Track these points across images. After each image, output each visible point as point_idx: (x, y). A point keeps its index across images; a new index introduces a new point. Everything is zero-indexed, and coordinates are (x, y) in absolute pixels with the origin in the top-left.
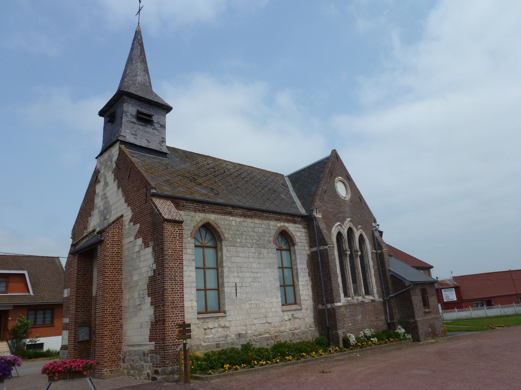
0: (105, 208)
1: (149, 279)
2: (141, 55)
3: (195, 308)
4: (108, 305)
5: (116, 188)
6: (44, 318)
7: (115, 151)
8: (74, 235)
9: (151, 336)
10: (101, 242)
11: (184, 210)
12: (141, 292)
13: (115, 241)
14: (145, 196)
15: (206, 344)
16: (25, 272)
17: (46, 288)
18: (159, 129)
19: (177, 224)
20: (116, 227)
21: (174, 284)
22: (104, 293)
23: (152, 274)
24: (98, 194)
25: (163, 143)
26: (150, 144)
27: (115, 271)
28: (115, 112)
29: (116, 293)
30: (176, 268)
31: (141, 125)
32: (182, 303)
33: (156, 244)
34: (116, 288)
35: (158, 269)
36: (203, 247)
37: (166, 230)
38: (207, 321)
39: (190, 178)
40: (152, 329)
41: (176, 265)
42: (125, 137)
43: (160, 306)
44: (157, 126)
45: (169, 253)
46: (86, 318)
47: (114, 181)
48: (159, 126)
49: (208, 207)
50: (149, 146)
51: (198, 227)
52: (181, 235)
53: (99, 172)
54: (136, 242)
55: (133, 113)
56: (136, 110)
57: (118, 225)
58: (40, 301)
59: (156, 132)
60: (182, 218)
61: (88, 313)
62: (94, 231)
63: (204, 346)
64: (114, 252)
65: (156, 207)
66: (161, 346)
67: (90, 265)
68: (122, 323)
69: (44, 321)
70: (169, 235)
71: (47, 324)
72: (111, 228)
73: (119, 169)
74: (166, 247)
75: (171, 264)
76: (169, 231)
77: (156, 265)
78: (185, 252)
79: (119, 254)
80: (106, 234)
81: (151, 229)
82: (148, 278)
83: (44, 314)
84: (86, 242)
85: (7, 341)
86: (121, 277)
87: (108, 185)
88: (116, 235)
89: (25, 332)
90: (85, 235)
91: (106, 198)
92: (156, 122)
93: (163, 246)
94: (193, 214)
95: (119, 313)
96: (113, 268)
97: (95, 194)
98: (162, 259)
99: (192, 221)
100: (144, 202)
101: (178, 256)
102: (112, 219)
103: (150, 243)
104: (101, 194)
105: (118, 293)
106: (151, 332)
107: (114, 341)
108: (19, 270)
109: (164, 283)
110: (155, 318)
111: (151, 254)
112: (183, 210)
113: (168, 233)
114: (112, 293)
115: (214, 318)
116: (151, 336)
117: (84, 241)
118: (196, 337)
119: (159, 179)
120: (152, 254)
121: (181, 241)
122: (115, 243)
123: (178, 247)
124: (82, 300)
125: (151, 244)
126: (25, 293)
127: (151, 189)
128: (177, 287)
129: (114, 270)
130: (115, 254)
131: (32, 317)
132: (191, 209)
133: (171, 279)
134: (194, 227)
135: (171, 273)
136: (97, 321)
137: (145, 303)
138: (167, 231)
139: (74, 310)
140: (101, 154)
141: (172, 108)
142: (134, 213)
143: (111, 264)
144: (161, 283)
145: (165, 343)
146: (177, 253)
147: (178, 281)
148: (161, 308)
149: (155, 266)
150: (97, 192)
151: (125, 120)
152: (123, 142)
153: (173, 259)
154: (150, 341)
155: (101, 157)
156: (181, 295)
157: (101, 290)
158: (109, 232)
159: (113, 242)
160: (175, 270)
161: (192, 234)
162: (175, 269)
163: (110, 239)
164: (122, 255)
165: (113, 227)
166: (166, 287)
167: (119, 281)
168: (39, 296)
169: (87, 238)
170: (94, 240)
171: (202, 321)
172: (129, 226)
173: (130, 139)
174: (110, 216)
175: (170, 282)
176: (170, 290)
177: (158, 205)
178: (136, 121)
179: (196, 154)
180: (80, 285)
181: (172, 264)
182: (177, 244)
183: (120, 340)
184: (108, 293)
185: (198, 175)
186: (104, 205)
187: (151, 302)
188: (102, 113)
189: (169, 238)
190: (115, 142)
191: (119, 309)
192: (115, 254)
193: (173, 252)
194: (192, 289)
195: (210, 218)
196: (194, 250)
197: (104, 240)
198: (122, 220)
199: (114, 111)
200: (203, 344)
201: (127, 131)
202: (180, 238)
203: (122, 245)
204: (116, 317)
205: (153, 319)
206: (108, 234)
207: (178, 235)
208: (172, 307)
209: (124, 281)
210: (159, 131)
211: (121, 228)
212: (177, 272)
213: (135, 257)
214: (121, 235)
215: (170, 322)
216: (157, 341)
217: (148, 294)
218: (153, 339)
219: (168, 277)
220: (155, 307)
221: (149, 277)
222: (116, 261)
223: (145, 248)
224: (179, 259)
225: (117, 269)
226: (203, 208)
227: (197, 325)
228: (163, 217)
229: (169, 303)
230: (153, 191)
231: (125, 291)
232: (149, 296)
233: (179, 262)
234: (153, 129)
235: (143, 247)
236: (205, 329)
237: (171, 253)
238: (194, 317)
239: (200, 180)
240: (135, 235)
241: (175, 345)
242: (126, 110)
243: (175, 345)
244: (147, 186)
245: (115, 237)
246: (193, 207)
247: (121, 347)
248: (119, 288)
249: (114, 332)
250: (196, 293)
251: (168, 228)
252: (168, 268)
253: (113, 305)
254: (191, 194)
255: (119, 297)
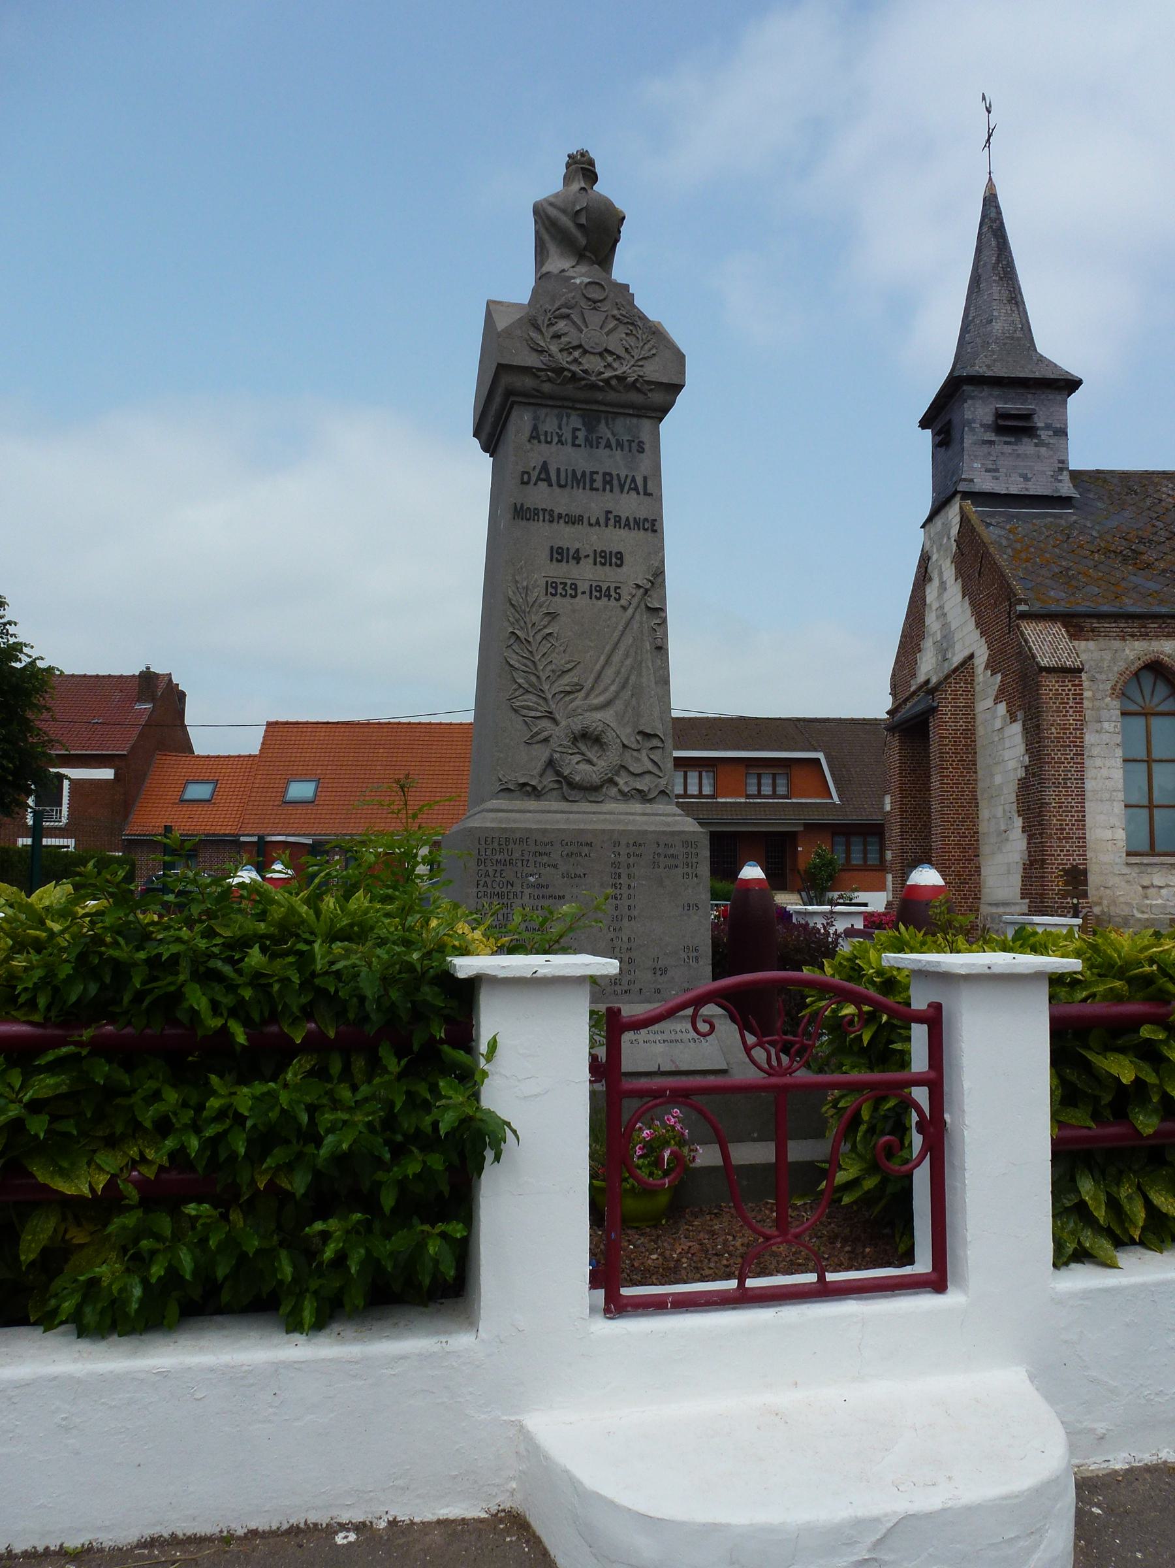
0: (944, 637)
1: (1019, 784)
2: (998, 261)
3: (1122, 844)
4: (950, 829)
5: (960, 595)
6: (865, 852)
7: (953, 513)
8: (895, 687)
9: (1024, 889)
10: (933, 710)
11: (1095, 638)
12: (1007, 807)
13: (959, 707)
14: (1006, 618)
15: (1146, 916)
16: (820, 755)
17: (864, 789)
18: (1051, 441)
19: (1069, 675)
20: (961, 680)
21: (1064, 795)
22: (943, 807)
23: (1024, 775)
24: (930, 606)
25: (1061, 475)
26: (1030, 485)
27: (962, 765)
28: (950, 422)
29: (965, 807)
30: (1069, 763)
31: (1006, 443)
32: (1081, 832)
33: (1028, 716)
34: (966, 797)
35: (1033, 765)
36: (1145, 715)
37: (1046, 690)
38: (1149, 871)
39: (1124, 553)
40: (1025, 877)
41: (1068, 757)
42: (972, 480)
43: (1035, 834)
44: (1044, 435)
45: (1052, 733)
46: (921, 853)
47: (956, 580)
48: (1051, 433)
49: (1156, 625)
50: (1027, 489)
51: (1131, 672)
52: (1078, 697)
53: (929, 558)
54: (995, 711)
55: (987, 420)
56: (994, 410)
57: (964, 676)
58: (853, 818)
59: (1043, 450)
60: (1081, 661)
61: (924, 842)
62: (927, 682)
63: (1139, 920)
64: (959, 730)
65: (1026, 641)
66: (1038, 907)
67: (923, 752)
68: (979, 864)
69: (865, 859)
70: (1051, 698)
71: (869, 865)
72: (951, 683)
73: (963, 555)
74: (1045, 723)
75: (1056, 757)
76: (1051, 690)
77: (1029, 757)
78: (1099, 729)
79: (970, 732)
80: (942, 695)
81: (1020, 686)
82: (1017, 781)
83: (865, 844)
84: (913, 706)
85: (799, 892)
86: (974, 778)
87: (945, 589)
88: (961, 695)
89: (831, 877)
90: (912, 689)
91: (945, 615)
92: (1043, 425)
93: (1038, 721)
94: (1117, 644)
95: (973, 844)
96: (958, 761)
97: (925, 604)
98: (1037, 745)
99: (1114, 660)
100: (1006, 630)
101: (1071, 739)
102: (957, 660)
103: (1018, 713)
104: (935, 606)
105: (970, 807)
106: (1023, 881)
107: (965, 895)
108: (809, 750)
109: (1041, 791)
110: (1029, 856)
111: (1020, 735)
112: (1092, 640)
113: (1049, 694)
114: (958, 807)
115: (1166, 866)
116: (1024, 889)
117: (909, 705)
118: (1122, 899)
119: (1043, 572)
120: (1022, 736)
121: (1078, 709)
122: (960, 711)
123: (1071, 722)
124: (913, 818)
125: (1020, 715)
126: (823, 798)
127: (1017, 604)
128: (1070, 800)
129: (960, 763)
130: (961, 734)
131: (840, 849)
132: (1111, 634)
133: (1057, 785)
134: (1120, 674)
135: (1057, 773)
136: (934, 857)
137: (1013, 828)
138: (1048, 692)
139: (899, 836)
140: (930, 519)
141: (1081, 380)
142: (992, 651)
143: (953, 753)
144: (1038, 792)
145: (1043, 902)
146: (1071, 733)
147: (1073, 789)
148: (1037, 838)
149: (1027, 758)
150: (928, 601)
151: (970, 441)
152: (966, 495)
153: (1062, 746)
154: (1022, 898)
155: (931, 525)
156: (1078, 816)
157: (938, 800)
158: (948, 691)
159: (956, 711)
160: (1067, 767)
161: (1115, 690)
162: (1066, 765)
163: (950, 705)
164: (974, 734)
165: (954, 679)
166: (1045, 799)
167: (971, 784)
168: (851, 806)
169: (915, 697)
170: (921, 707)
171: (1136, 870)
172: (984, 677)
173: (984, 483)
174: (954, 654)
175: (1054, 791)
176: (1054, 805)
177: (1031, 638)
178: (993, 439)
179: (1158, 473)
180: (907, 790)
181: (1059, 756)
182: (1071, 716)
183: (976, 894)
184: (950, 807)
185: (1150, 541)
186: (941, 630)
187: (1023, 827)
188: (925, 423)
189: (1052, 705)
190: (956, 493)
191: (971, 837)
192: (961, 734)
193: (1062, 731)
194: (1115, 804)
195: (1162, 649)
196: (1119, 724)
197: (938, 706)
198: (973, 665)
199: (947, 419)
200: (1139, 915)
201: (975, 465)
202: (1076, 703)
203: (974, 715)
204: (968, 852)
205: (1026, 857)
206: (946, 695)
207: (1071, 697)
208: (1059, 838)
209: (980, 785)
210: (1051, 446)
211: (971, 680)
212: (1070, 771)
213: (996, 739)
214: (970, 694)
215: (1056, 866)
216: (1032, 898)
217: (1019, 811)
218: (1027, 894)
219: (1051, 782)
220: (1028, 835)
221: (1019, 780)
222: (964, 745)
223: (1011, 723)
224: (1074, 746)
225: (965, 761)
226: (1143, 630)
227: (1125, 877)
228: (1038, 664)
229: (1052, 829)
230: (1022, 608)
231: (983, 804)
232: (1019, 816)
233: (1074, 752)
234: (1036, 445)
235: (1008, 720)
236: (1144, 887)
237: (1055, 735)
238: (1118, 860)
239: (1150, 556)
240: (994, 697)
241: (1064, 907)
242: (971, 417)
243: (1064, 907)
244: (1011, 597)
245: (959, 699)
246: (1118, 630)
247: (978, 907)
248: (970, 797)
249: (965, 879)
250: (1123, 812)
251: (1051, 683)
252: (1051, 763)
253: (961, 829)
254: (1116, 598)
255: (972, 814)
